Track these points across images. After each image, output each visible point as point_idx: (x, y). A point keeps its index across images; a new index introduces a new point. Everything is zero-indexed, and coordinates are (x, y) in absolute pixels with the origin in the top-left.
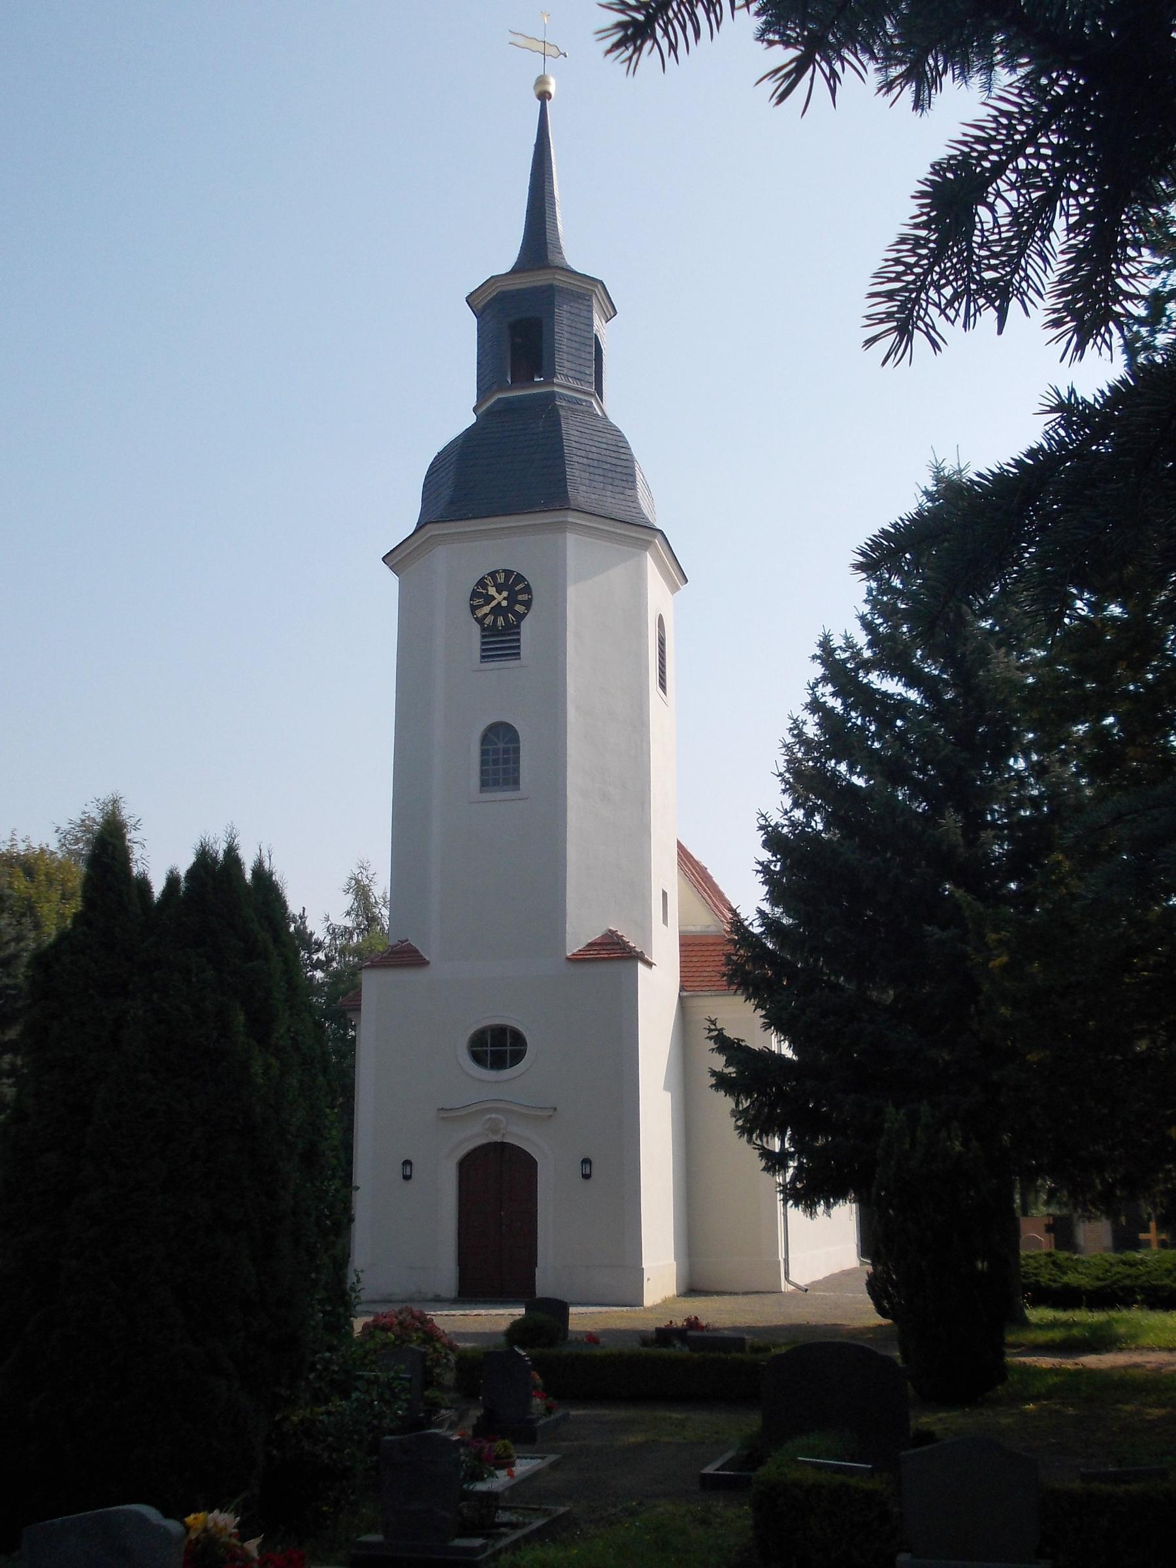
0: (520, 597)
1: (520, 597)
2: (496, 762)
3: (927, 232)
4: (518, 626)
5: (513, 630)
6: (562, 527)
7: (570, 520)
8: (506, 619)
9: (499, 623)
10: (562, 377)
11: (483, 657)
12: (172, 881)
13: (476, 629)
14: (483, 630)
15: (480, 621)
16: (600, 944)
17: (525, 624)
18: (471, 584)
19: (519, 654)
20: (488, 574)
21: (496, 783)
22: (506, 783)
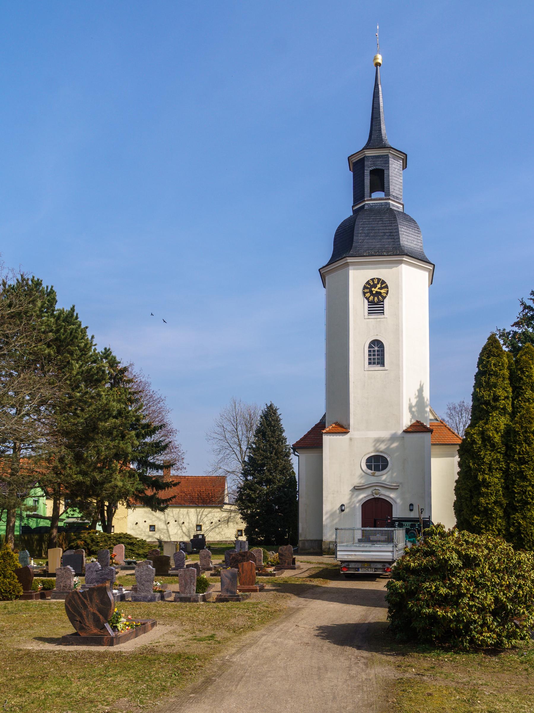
0: (372, 284)
1: (372, 284)
2: (374, 355)
3: (61, 505)
4: (383, 301)
5: (381, 302)
6: (401, 262)
7: (404, 259)
8: (378, 298)
9: (375, 300)
10: (309, 436)
11: (369, 313)
12: (116, 507)
13: (366, 301)
14: (369, 302)
15: (367, 299)
16: (415, 426)
17: (386, 301)
18: (382, 278)
19: (383, 313)
20: (371, 280)
21: (374, 363)
22: (378, 363)
